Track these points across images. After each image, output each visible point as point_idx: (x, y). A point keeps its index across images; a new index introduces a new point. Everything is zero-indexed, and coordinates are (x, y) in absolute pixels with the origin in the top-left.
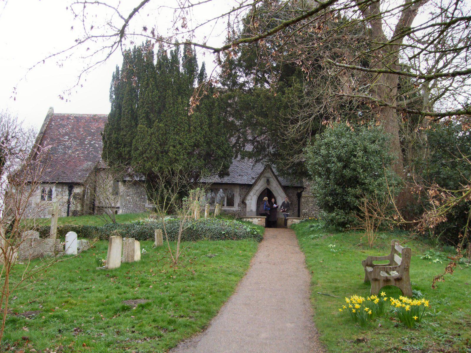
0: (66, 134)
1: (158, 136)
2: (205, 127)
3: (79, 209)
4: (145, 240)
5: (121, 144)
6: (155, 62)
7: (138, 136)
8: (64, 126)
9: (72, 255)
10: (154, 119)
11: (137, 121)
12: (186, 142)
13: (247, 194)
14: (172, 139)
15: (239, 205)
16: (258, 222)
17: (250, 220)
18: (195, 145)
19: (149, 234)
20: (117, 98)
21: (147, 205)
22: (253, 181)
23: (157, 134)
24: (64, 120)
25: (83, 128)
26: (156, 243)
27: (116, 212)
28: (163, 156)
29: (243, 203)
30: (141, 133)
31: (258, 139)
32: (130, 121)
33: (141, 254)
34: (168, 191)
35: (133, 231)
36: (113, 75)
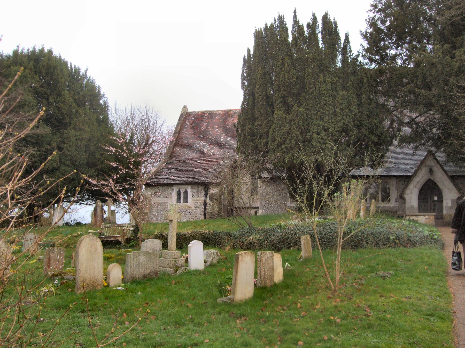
0: (201, 132)
1: (298, 122)
2: (354, 108)
3: (216, 210)
4: (288, 248)
5: (257, 136)
6: (290, 39)
7: (275, 124)
8: (198, 124)
9: (197, 271)
10: (292, 103)
11: (273, 108)
12: (332, 127)
13: (406, 186)
14: (315, 125)
15: (396, 200)
16: (425, 220)
17: (415, 218)
18: (343, 131)
19: (293, 241)
20: (249, 85)
21: (289, 204)
22: (413, 171)
23: (297, 120)
24: (198, 118)
25: (218, 125)
26: (303, 254)
27: (256, 213)
28: (305, 146)
29: (401, 197)
30: (279, 120)
31: (417, 120)
32: (266, 108)
33: (284, 270)
34: (318, 183)
35: (273, 237)
36: (244, 59)
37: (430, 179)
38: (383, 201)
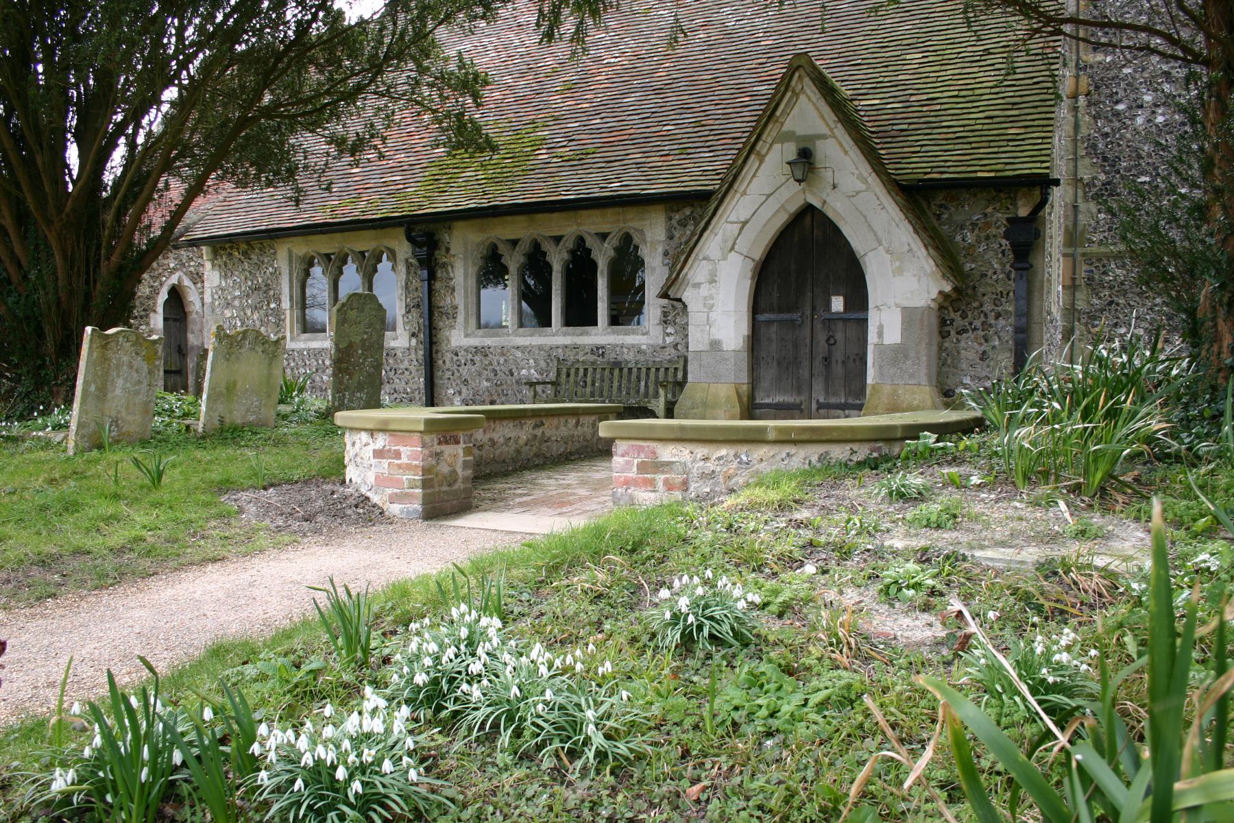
37: (808, 209)
38: (615, 321)
